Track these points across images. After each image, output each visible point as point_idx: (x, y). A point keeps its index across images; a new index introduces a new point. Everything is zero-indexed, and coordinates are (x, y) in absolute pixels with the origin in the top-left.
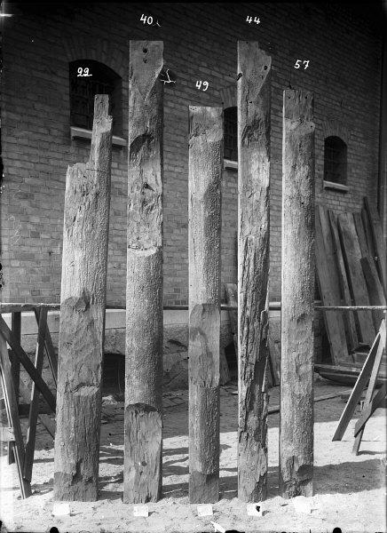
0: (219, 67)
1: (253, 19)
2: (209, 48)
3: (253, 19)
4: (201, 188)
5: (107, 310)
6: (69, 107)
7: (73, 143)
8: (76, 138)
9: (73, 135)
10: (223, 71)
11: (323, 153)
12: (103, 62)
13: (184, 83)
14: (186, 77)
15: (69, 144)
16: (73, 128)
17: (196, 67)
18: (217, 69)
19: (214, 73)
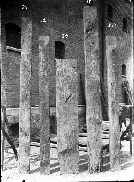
0: (53, 27)
1: (65, 35)
2: (50, 21)
3: (65, 35)
4: (95, 13)
5: (32, 108)
6: (5, 39)
7: (7, 51)
8: (8, 50)
9: (7, 48)
10: (55, 29)
11: (54, 48)
12: (14, 23)
13: (42, 32)
14: (43, 30)
15: (6, 52)
16: (7, 46)
17: (46, 27)
18: (53, 28)
19: (52, 29)
